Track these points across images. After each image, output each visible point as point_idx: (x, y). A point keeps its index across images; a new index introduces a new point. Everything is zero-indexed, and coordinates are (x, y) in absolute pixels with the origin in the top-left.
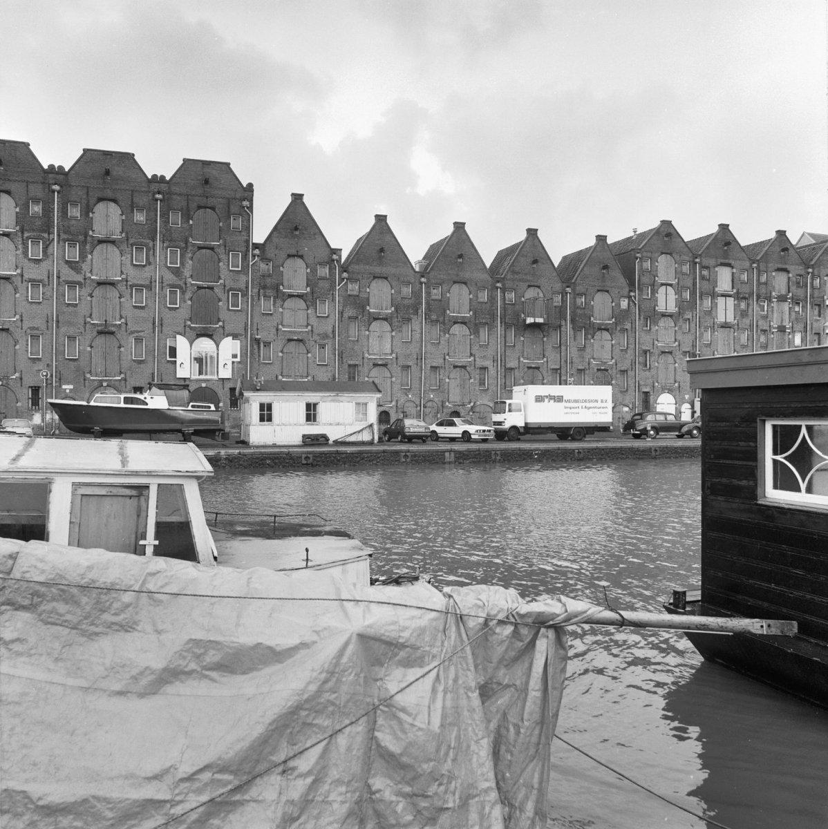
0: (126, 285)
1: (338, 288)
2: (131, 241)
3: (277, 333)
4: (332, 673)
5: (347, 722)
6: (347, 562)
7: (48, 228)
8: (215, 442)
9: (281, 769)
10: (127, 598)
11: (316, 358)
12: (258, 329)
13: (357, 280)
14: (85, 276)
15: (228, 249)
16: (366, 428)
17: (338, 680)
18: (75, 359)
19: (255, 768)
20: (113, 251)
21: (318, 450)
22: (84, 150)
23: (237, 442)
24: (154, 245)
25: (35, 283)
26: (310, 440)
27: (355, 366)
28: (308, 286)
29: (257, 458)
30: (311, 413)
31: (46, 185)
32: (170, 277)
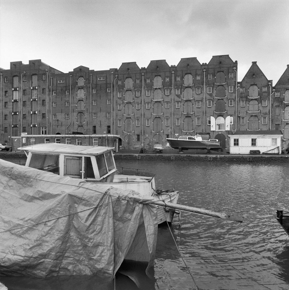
0: (194, 101)
1: (271, 95)
2: (196, 86)
3: (247, 114)
4: (60, 203)
5: (63, 216)
6: (139, 182)
8: (218, 153)
9: (44, 223)
10: (32, 180)
11: (262, 122)
12: (239, 113)
13: (279, 91)
14: (182, 99)
15: (228, 85)
16: (276, 148)
17: (61, 205)
18: (139, 126)
19: (39, 222)
20: (190, 90)
21: (254, 156)
22: (151, 61)
23: (227, 153)
24: (203, 87)
25: (167, 102)
26: (252, 152)
27: (279, 124)
28: (259, 95)
29: (231, 158)
30: (254, 143)
31: (170, 72)
32: (208, 97)
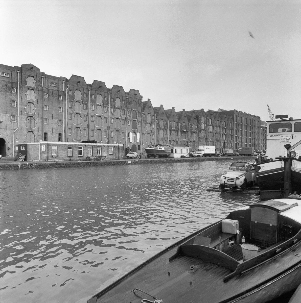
7: (108, 104)
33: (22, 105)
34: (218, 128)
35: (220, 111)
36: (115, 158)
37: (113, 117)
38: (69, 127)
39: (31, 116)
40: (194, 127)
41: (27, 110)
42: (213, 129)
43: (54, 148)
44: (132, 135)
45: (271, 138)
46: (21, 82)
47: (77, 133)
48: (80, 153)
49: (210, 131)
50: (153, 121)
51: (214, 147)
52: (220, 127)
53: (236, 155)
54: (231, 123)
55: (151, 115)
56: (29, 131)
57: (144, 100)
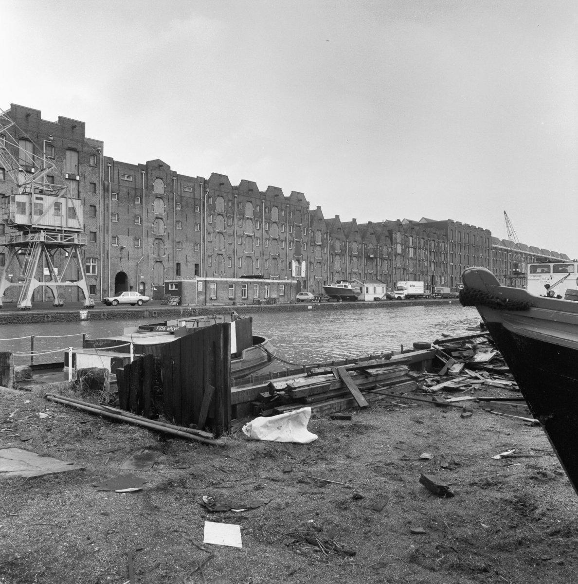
7: (261, 217)
33: (148, 221)
34: (424, 251)
35: (425, 222)
36: (286, 300)
37: (268, 237)
38: (209, 253)
39: (159, 239)
40: (385, 250)
41: (154, 229)
42: (415, 253)
43: (213, 286)
44: (294, 264)
45: (532, 278)
46: (147, 188)
47: (219, 263)
48: (243, 293)
49: (410, 256)
50: (325, 241)
51: (421, 284)
52: (426, 250)
53: (455, 296)
54: (444, 242)
55: (323, 232)
56: (157, 262)
57: (312, 207)
